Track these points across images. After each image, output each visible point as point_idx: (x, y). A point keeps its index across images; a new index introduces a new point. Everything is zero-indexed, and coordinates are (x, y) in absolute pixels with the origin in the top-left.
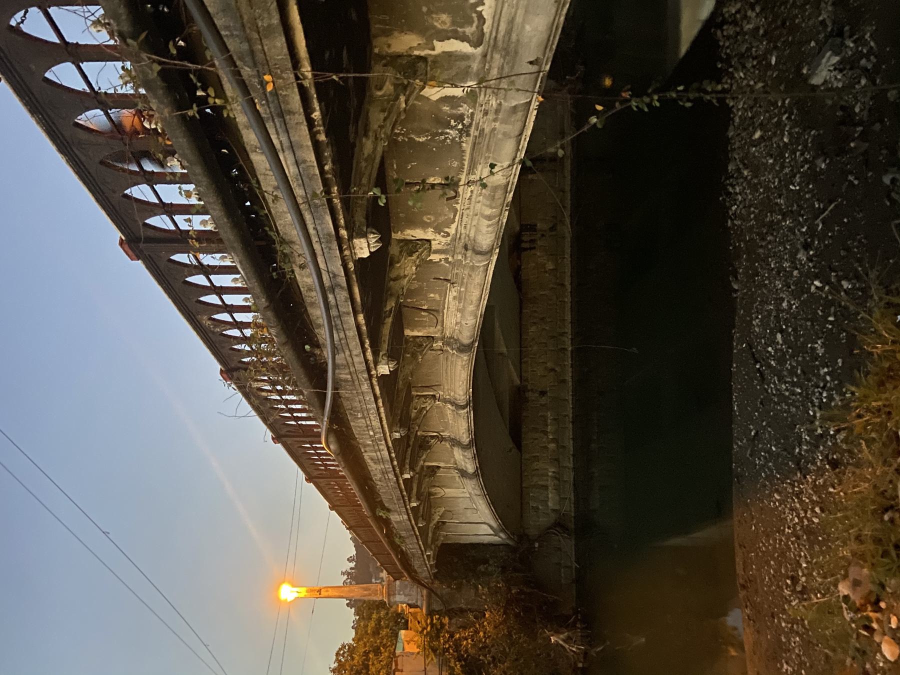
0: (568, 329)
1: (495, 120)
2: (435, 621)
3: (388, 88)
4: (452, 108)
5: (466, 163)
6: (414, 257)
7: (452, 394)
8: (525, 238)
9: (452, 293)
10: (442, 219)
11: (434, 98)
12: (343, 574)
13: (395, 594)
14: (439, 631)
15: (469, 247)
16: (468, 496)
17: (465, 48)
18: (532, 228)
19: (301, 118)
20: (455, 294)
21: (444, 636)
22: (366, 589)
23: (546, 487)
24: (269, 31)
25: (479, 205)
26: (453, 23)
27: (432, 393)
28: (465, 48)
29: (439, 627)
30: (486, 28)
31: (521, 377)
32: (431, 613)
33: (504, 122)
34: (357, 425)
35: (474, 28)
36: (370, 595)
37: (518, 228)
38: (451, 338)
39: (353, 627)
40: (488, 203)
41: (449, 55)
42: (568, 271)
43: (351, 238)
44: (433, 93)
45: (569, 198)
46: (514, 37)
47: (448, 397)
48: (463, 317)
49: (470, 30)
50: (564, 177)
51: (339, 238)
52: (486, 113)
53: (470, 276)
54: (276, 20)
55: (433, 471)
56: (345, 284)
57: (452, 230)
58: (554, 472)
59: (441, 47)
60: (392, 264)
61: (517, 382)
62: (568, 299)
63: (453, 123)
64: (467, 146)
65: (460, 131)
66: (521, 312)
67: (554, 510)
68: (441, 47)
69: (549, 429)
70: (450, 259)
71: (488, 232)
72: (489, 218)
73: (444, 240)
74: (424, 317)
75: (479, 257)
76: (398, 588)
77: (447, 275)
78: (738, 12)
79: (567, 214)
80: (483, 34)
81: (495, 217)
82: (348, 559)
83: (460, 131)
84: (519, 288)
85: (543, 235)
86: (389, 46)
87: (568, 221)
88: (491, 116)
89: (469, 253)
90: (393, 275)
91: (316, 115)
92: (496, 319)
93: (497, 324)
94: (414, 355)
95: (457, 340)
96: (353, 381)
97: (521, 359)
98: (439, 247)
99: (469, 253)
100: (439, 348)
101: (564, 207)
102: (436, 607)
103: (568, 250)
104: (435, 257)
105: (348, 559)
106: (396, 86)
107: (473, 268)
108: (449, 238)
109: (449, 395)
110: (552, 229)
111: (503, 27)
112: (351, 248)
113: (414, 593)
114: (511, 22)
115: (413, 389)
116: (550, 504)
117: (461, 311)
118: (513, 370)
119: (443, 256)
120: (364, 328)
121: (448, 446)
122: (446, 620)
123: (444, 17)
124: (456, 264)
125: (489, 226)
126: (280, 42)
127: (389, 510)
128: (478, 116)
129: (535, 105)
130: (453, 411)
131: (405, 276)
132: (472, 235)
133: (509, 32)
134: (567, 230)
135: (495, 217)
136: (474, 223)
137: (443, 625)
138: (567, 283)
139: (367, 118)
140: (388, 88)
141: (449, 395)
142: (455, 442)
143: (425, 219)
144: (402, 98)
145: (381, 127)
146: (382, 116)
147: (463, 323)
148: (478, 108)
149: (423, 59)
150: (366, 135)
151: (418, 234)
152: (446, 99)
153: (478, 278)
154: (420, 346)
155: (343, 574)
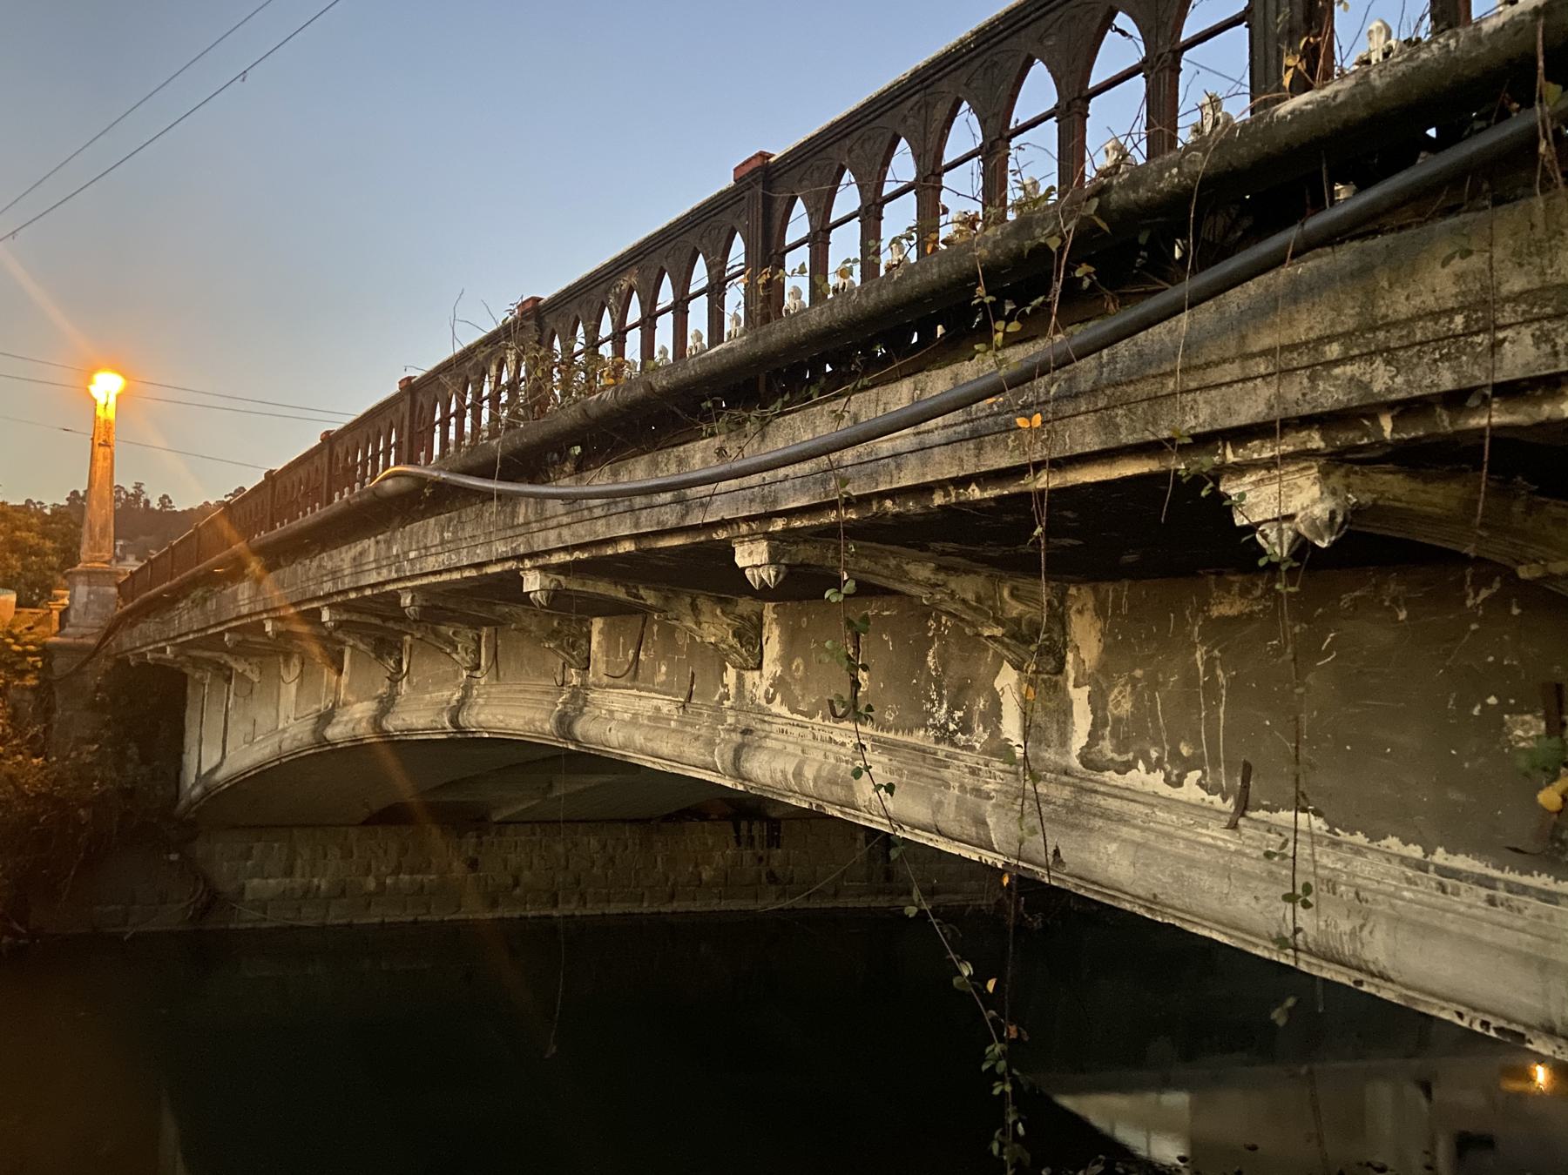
1: (962, 787)
2: (30, 659)
3: (1015, 609)
5: (891, 735)
6: (732, 641)
7: (481, 701)
9: (666, 705)
10: (797, 691)
12: (138, 486)
13: (89, 584)
15: (748, 738)
16: (280, 727)
18: (774, 840)
19: (970, 469)
20: (665, 710)
23: (289, 872)
24: (1110, 426)
25: (821, 757)
26: (1118, 720)
27: (483, 663)
28: (1079, 739)
29: (18, 667)
30: (1110, 776)
31: (505, 823)
32: (46, 652)
33: (960, 802)
34: (431, 529)
36: (91, 538)
37: (773, 815)
38: (585, 700)
39: (29, 501)
40: (824, 774)
42: (696, 907)
43: (769, 536)
44: (1007, 680)
46: (1099, 823)
49: (1106, 747)
52: (974, 772)
53: (697, 738)
54: (1126, 438)
57: (777, 707)
58: (319, 887)
59: (1079, 697)
60: (720, 601)
61: (496, 817)
62: (645, 908)
63: (958, 714)
64: (919, 737)
65: (944, 727)
66: (624, 821)
67: (243, 889)
68: (1079, 697)
70: (727, 704)
71: (773, 771)
72: (798, 774)
73: (760, 692)
74: (626, 655)
75: (729, 755)
76: (102, 590)
79: (798, 902)
80: (1101, 770)
81: (800, 785)
82: (165, 497)
83: (944, 727)
84: (668, 818)
85: (761, 859)
86: (1080, 612)
87: (786, 903)
88: (969, 781)
89: (737, 737)
91: (975, 493)
96: (513, 527)
98: (748, 685)
99: (737, 737)
102: (60, 663)
103: (734, 905)
104: (730, 676)
105: (165, 497)
106: (1017, 621)
107: (710, 743)
108: (763, 702)
110: (772, 878)
111: (1113, 804)
112: (752, 537)
113: (90, 621)
114: (1121, 819)
116: (256, 881)
117: (634, 721)
119: (732, 691)
122: (31, 681)
123: (1127, 706)
124: (718, 715)
125: (784, 773)
126: (1092, 443)
128: (969, 759)
131: (699, 624)
132: (769, 743)
133: (1105, 815)
134: (770, 902)
135: (800, 785)
137: (22, 674)
140: (1015, 609)
141: (479, 696)
142: (387, 705)
143: (798, 661)
146: (970, 596)
147: (613, 724)
149: (1061, 663)
151: (772, 648)
153: (693, 752)
154: (573, 646)
155: (138, 486)
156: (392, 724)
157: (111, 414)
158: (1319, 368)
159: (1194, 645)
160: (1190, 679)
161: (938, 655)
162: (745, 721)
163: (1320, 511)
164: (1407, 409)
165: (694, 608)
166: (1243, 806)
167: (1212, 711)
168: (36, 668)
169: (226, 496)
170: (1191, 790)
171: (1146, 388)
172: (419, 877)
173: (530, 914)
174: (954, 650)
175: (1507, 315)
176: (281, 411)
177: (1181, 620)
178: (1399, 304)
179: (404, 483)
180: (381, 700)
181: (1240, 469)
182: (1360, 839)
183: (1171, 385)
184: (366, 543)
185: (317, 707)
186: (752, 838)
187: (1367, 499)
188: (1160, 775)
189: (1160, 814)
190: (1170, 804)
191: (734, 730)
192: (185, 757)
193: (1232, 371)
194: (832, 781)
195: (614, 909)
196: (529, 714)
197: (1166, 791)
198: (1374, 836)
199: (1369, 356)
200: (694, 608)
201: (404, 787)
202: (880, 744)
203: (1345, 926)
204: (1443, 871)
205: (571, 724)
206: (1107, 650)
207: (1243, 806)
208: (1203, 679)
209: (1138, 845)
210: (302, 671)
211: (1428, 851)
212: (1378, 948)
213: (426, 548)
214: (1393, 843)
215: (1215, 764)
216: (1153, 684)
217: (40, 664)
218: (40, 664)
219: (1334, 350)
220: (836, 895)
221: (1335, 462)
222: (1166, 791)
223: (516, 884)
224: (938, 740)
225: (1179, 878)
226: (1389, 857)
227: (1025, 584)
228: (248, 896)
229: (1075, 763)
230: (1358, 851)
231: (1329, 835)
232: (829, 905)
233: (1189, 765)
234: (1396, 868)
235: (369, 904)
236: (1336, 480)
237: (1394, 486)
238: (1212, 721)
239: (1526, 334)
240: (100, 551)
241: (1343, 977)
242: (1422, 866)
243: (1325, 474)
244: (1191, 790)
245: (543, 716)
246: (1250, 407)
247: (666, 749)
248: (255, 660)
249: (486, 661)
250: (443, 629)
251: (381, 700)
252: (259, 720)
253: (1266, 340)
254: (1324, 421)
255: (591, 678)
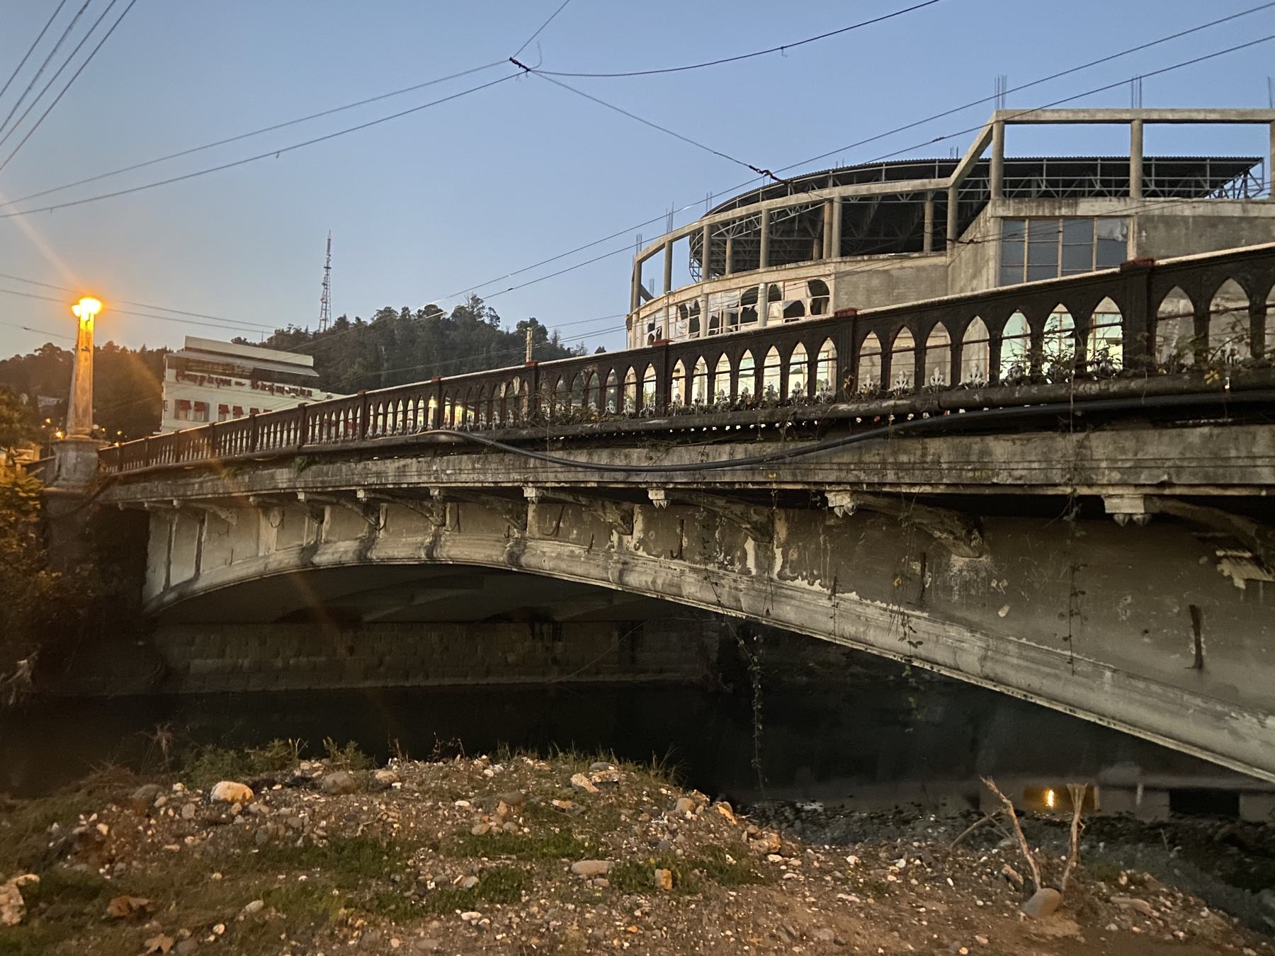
0: (432, 682)
1: (730, 587)
2: (32, 503)
3: (755, 518)
4: (739, 558)
5: (698, 566)
6: (620, 521)
7: (448, 543)
8: (545, 627)
9: (577, 550)
10: (651, 545)
11: (746, 546)
13: (78, 450)
14: (18, 509)
15: (626, 566)
16: (261, 554)
17: (777, 568)
18: (556, 636)
19: (750, 480)
20: (577, 552)
21: (11, 515)
22: (85, 411)
23: (222, 654)
24: (794, 475)
25: (664, 574)
26: (792, 561)
27: (448, 522)
28: (777, 568)
29: (24, 508)
30: (789, 582)
31: (374, 622)
32: (43, 497)
33: (729, 594)
34: (465, 461)
35: (789, 574)
36: (77, 416)
37: (557, 618)
38: (526, 547)
40: (667, 582)
41: (774, 558)
42: (504, 680)
43: (665, 489)
44: (750, 545)
45: (589, 680)
46: (783, 599)
47: (443, 539)
48: (551, 558)
49: (788, 571)
50: (612, 674)
51: (667, 483)
52: (735, 581)
53: (598, 566)
54: (799, 479)
55: (318, 516)
56: (630, 480)
57: (640, 552)
58: (242, 666)
59: (778, 552)
60: (615, 503)
61: (367, 618)
62: (469, 681)
63: (728, 558)
64: (710, 567)
65: (723, 563)
66: (455, 622)
67: (188, 667)
68: (778, 552)
69: (304, 660)
70: (612, 550)
71: (640, 581)
72: (654, 582)
73: (631, 546)
74: (551, 523)
75: (616, 574)
76: (86, 454)
77: (597, 546)
78: (786, 818)
79: (572, 677)
80: (785, 580)
81: (654, 586)
83: (723, 563)
84: (487, 620)
85: (547, 648)
86: (780, 519)
87: (564, 679)
88: (733, 584)
89: (620, 566)
90: (606, 503)
91: (750, 486)
92: (465, 591)
93: (454, 593)
94: (509, 512)
95: (523, 552)
96: (525, 468)
97: (397, 623)
98: (625, 542)
99: (620, 566)
100: (511, 533)
101: (578, 675)
102: (53, 507)
103: (529, 679)
104: (615, 537)
106: (756, 522)
107: (606, 569)
108: (633, 550)
109: (446, 541)
110: (555, 661)
111: (789, 592)
112: (658, 488)
113: (78, 475)
114: (792, 597)
115: (455, 504)
116: (197, 661)
117: (559, 556)
118: (386, 612)
119: (616, 544)
120: (582, 485)
121: (360, 535)
122: (33, 518)
123: (796, 556)
124: (608, 555)
125: (646, 582)
126: (789, 478)
127: (301, 470)
128: (733, 576)
129: (739, 614)
130: (422, 544)
131: (605, 514)
132: (637, 569)
133: (786, 596)
134: (554, 678)
135: (654, 586)
136: (649, 571)
137: (27, 513)
138: (491, 680)
139: (738, 503)
140: (755, 518)
141: (446, 541)
142: (368, 543)
143: (652, 532)
144: (748, 526)
145: (732, 512)
146: (738, 513)
147: (545, 558)
148: (739, 576)
149: (772, 538)
150: (727, 502)
151: (639, 525)
152: (745, 554)
153: (595, 572)
154: (518, 518)
156: (375, 555)
157: (91, 327)
158: (849, 471)
159: (820, 535)
160: (818, 547)
161: (721, 533)
162: (623, 558)
163: (850, 506)
164: (869, 484)
165: (603, 506)
166: (834, 592)
167: (825, 558)
168: (35, 509)
169: (36, 351)
170: (817, 587)
171: (806, 466)
172: (313, 659)
173: (390, 685)
174: (727, 531)
175: (889, 467)
176: (195, 319)
177: (816, 525)
178: (867, 458)
179: (460, 440)
180: (362, 540)
181: (831, 491)
182: (869, 602)
183: (812, 466)
184: (409, 461)
185: (299, 543)
186: (542, 634)
187: (862, 502)
188: (806, 581)
189: (806, 596)
190: (809, 592)
191: (618, 562)
192: (149, 574)
193: (827, 466)
194: (671, 585)
195: (447, 681)
196: (488, 552)
197: (808, 587)
198: (873, 601)
199: (860, 470)
200: (603, 506)
201: (310, 599)
202: (692, 569)
203: (862, 629)
204: (892, 611)
205: (518, 557)
206: (789, 534)
207: (834, 592)
208: (823, 547)
209: (798, 607)
210: (282, 520)
211: (888, 605)
212: (871, 636)
213: (460, 470)
214: (878, 603)
215: (825, 577)
216: (805, 548)
217: (39, 506)
218: (39, 506)
219: (852, 467)
220: (598, 673)
221: (853, 493)
222: (808, 587)
223: (380, 664)
224: (719, 568)
225: (810, 617)
226: (876, 607)
227: (760, 508)
228: (192, 671)
229: (775, 577)
230: (868, 606)
231: (461, 433)
232: (593, 680)
233: (817, 578)
234: (878, 611)
235: (278, 677)
236: (854, 497)
237: (870, 499)
238: (825, 564)
239: (893, 472)
240: (82, 426)
241: (861, 647)
242: (885, 610)
243: (851, 495)
244: (817, 587)
245: (498, 553)
246: (832, 478)
247: (579, 571)
248: (234, 510)
249: (451, 522)
250: (425, 503)
251: (362, 540)
252: (237, 549)
253: (835, 460)
254: (851, 484)
255: (527, 534)
